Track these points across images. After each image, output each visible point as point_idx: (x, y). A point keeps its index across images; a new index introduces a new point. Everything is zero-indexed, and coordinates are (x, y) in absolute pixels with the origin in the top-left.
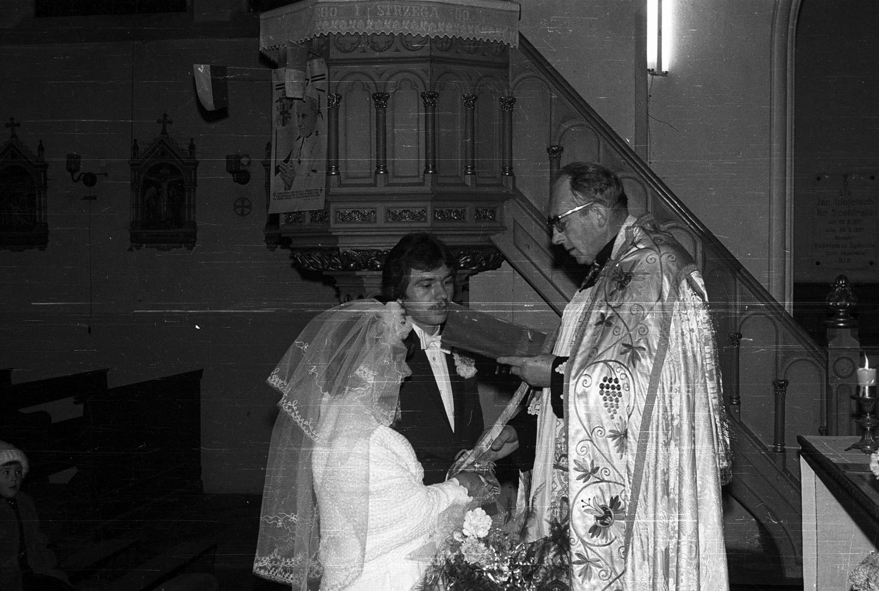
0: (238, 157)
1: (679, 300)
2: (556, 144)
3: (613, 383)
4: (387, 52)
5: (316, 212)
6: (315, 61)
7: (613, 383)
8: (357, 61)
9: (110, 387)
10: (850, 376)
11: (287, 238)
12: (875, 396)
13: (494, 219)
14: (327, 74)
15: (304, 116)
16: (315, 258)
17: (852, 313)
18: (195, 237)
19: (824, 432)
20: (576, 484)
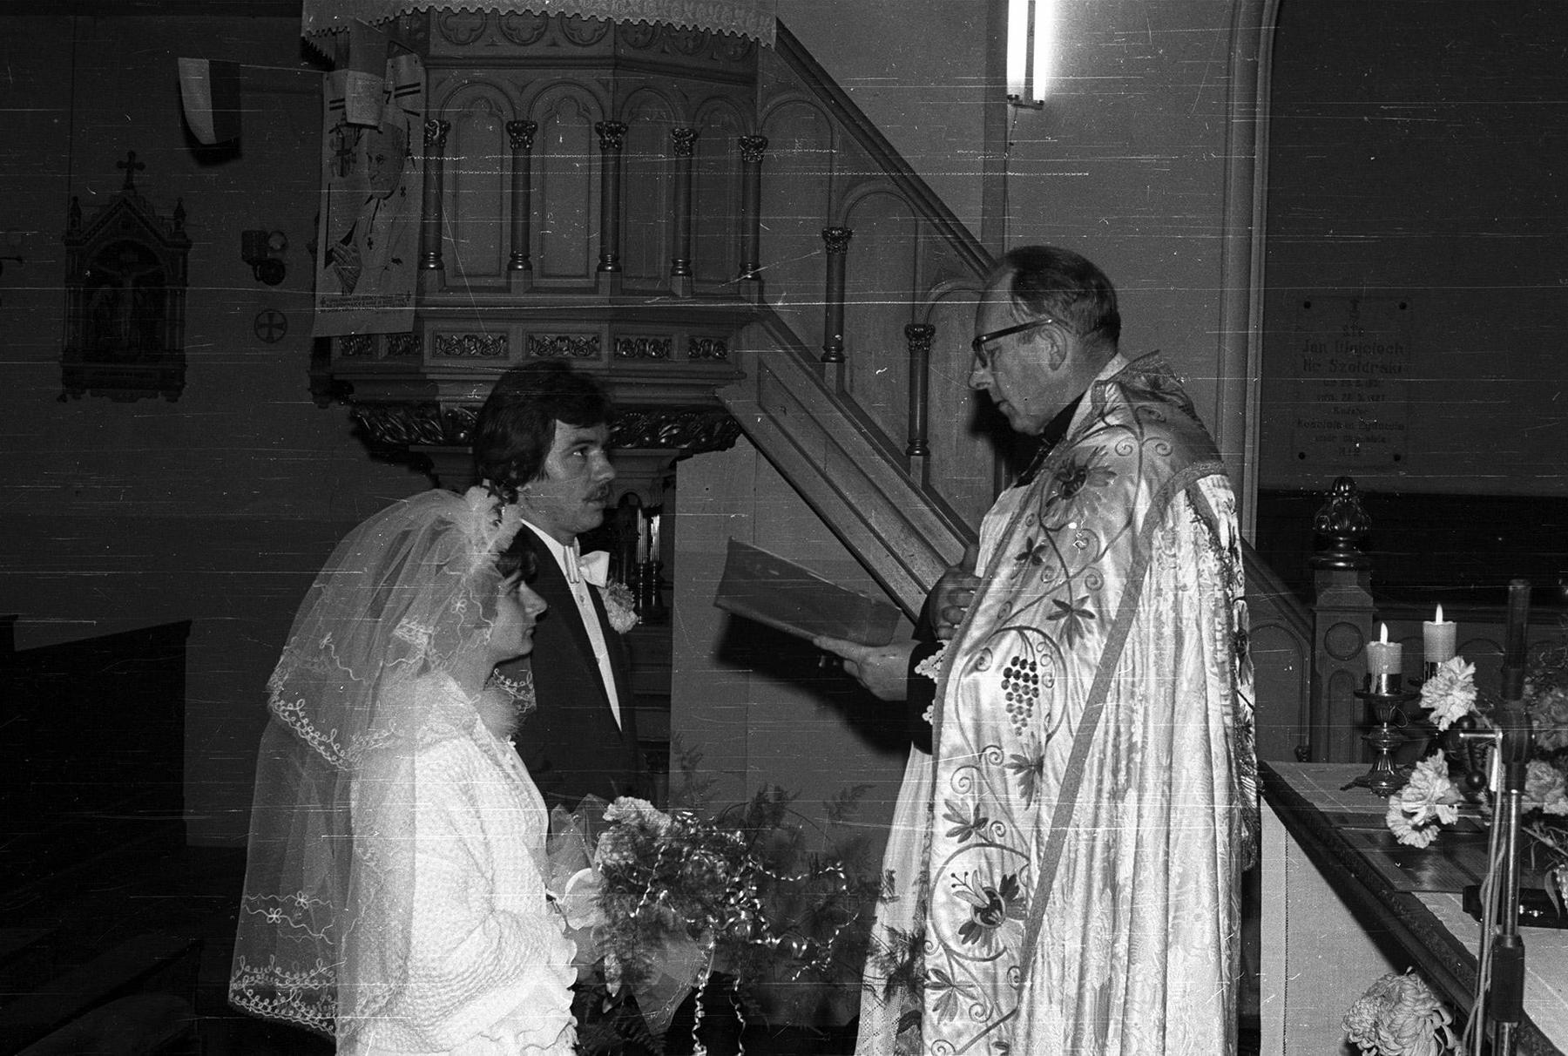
0: (264, 237)
1: (1163, 528)
2: (840, 223)
3: (1027, 670)
4: (537, 45)
5: (397, 336)
6: (403, 58)
7: (1027, 670)
8: (483, 62)
9: (18, 648)
10: (1355, 655)
11: (344, 382)
12: (1398, 692)
13: (722, 359)
14: (423, 84)
15: (379, 159)
16: (396, 419)
17: (1360, 542)
18: (182, 378)
19: (1306, 755)
20: (945, 847)
